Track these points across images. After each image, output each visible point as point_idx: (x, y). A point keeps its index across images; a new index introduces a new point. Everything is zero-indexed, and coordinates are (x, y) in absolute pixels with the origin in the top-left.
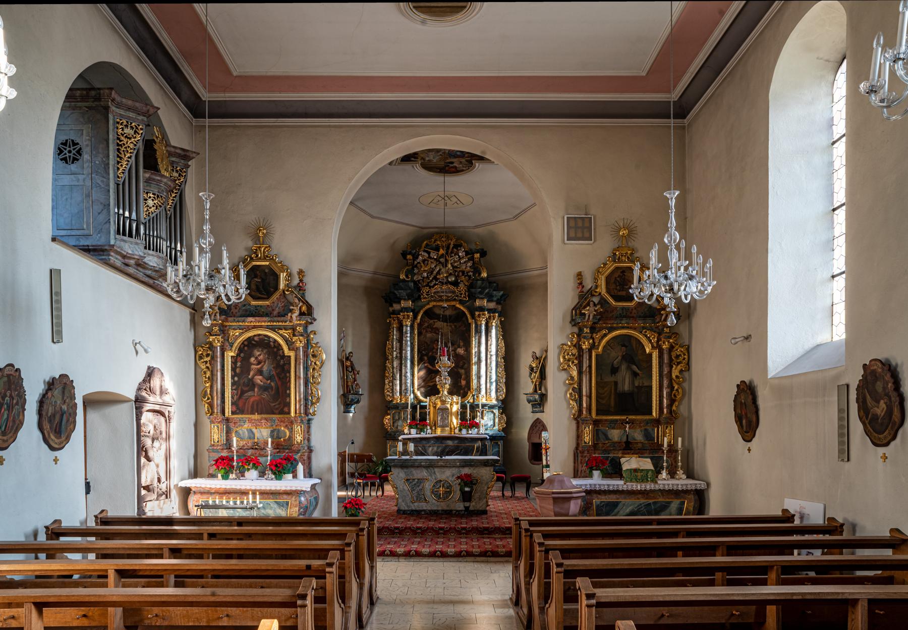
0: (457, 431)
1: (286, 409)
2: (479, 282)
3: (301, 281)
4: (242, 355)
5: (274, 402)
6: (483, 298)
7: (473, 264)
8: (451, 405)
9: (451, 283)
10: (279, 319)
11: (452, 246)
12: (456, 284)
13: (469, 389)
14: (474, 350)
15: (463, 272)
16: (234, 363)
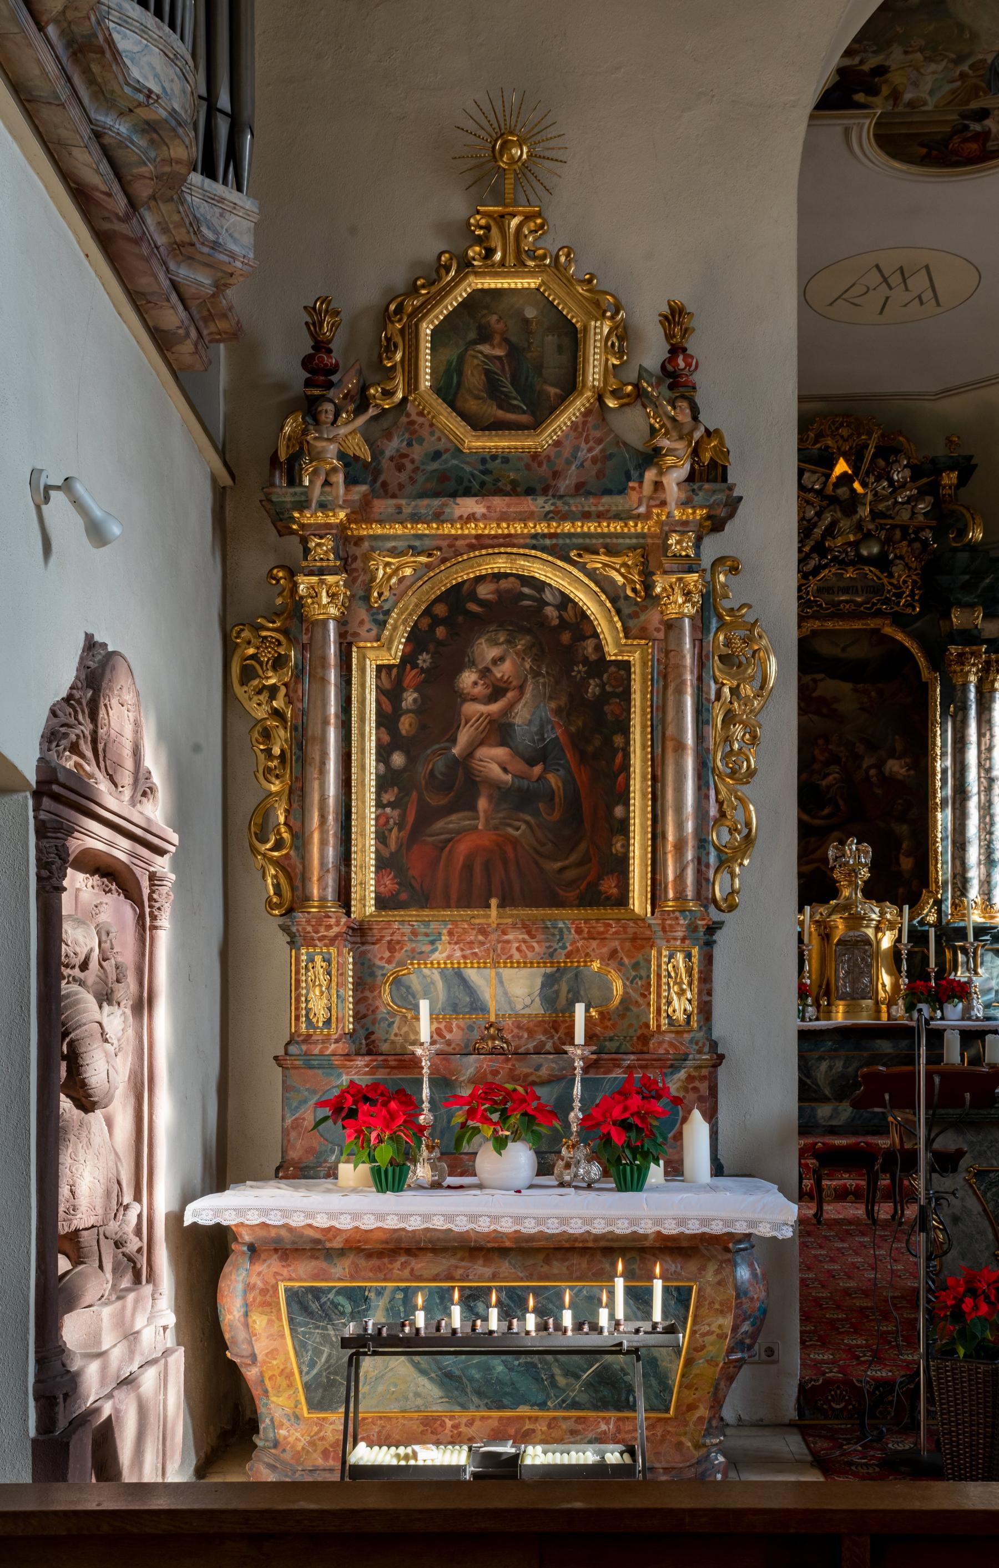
0: (899, 1010)
1: (609, 886)
2: (963, 556)
3: (676, 350)
4: (424, 660)
5: (561, 849)
6: (972, 606)
7: (937, 505)
8: (878, 929)
9: (869, 561)
10: (589, 504)
11: (871, 450)
12: (882, 562)
13: (925, 884)
14: (942, 763)
15: (904, 528)
16: (390, 693)
